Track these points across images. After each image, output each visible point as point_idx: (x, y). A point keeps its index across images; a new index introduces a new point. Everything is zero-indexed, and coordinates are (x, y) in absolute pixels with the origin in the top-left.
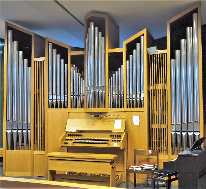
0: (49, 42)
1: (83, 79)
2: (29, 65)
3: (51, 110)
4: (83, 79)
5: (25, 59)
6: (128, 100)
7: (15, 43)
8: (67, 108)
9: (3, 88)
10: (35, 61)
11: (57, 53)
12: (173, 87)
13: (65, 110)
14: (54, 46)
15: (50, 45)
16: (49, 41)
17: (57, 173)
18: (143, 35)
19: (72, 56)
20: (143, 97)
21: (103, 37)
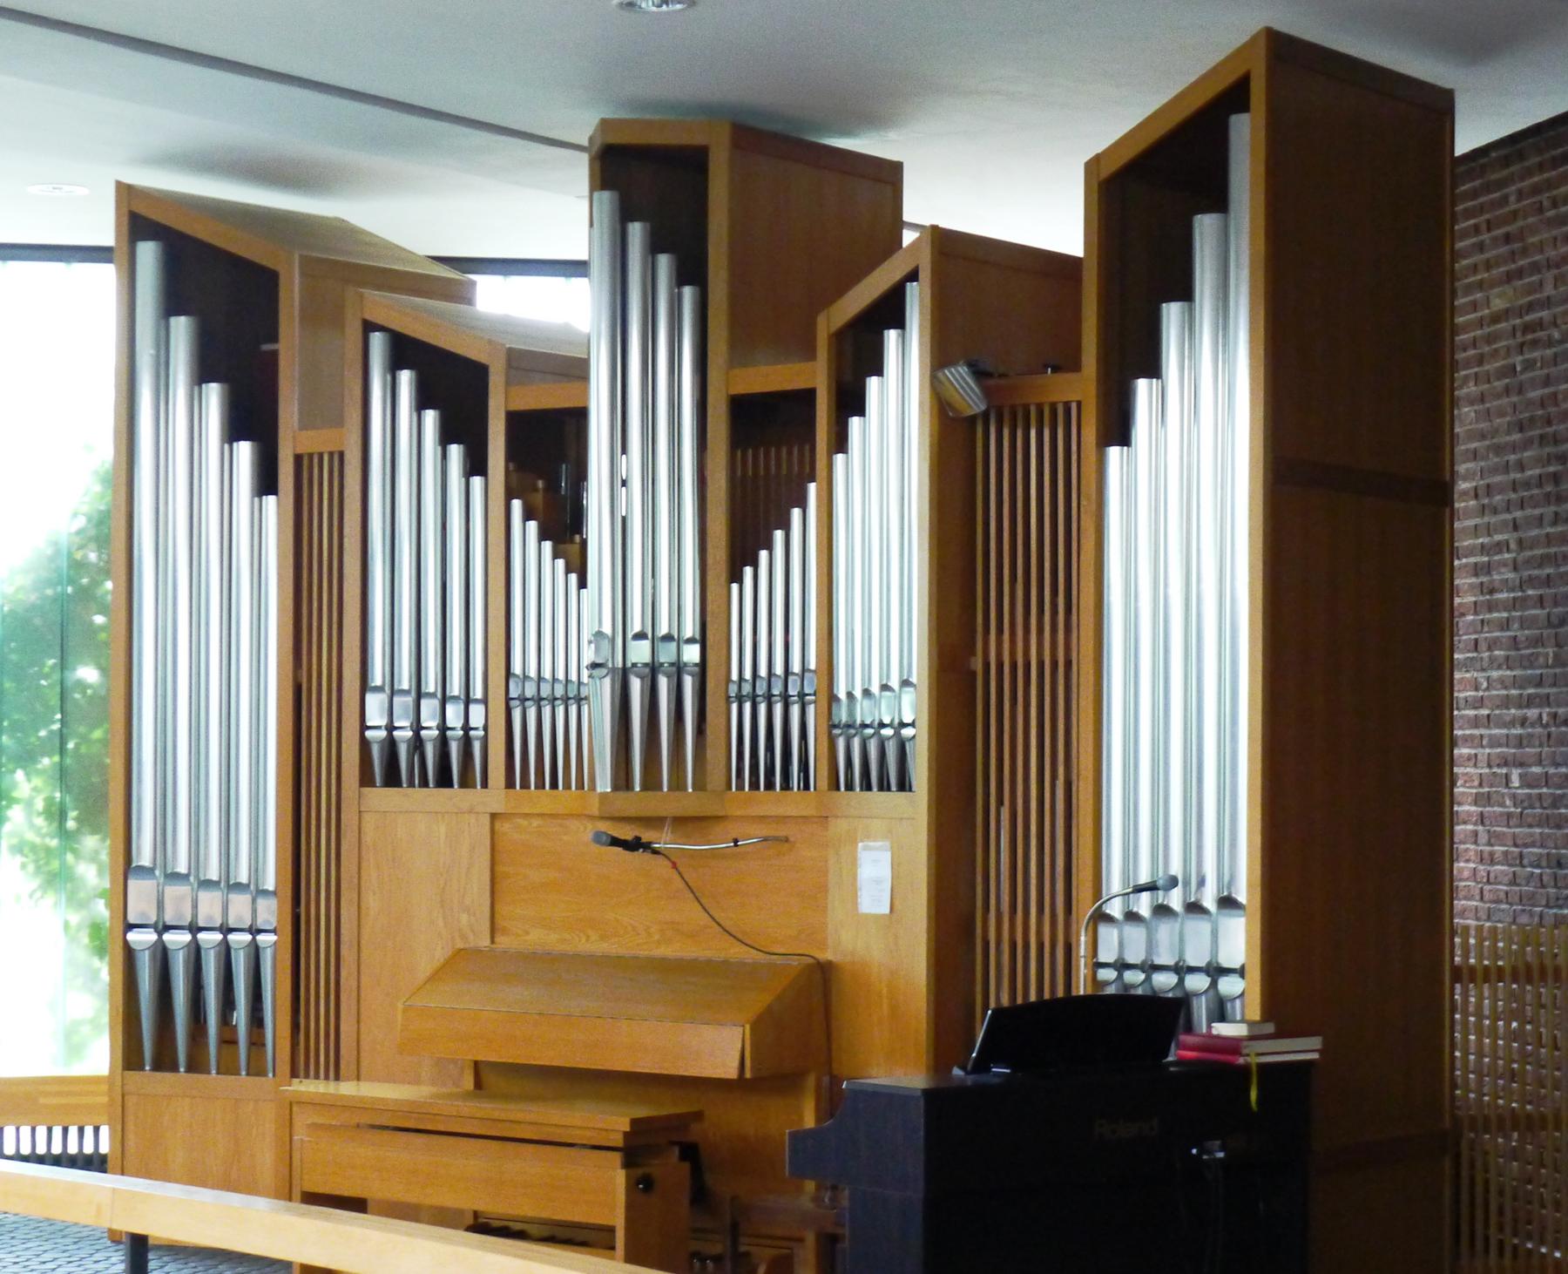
0: (369, 327)
1: (582, 584)
2: (266, 483)
3: (381, 797)
4: (582, 584)
5: (238, 440)
6: (887, 732)
7: (181, 326)
8: (485, 785)
9: (577, 538)
10: (299, 451)
11: (423, 401)
12: (604, 769)
13: (475, 795)
14: (405, 351)
15: (377, 341)
16: (368, 317)
17: (151, 1242)
18: (913, 276)
19: (516, 420)
20: (132, 883)
21: (688, 292)
